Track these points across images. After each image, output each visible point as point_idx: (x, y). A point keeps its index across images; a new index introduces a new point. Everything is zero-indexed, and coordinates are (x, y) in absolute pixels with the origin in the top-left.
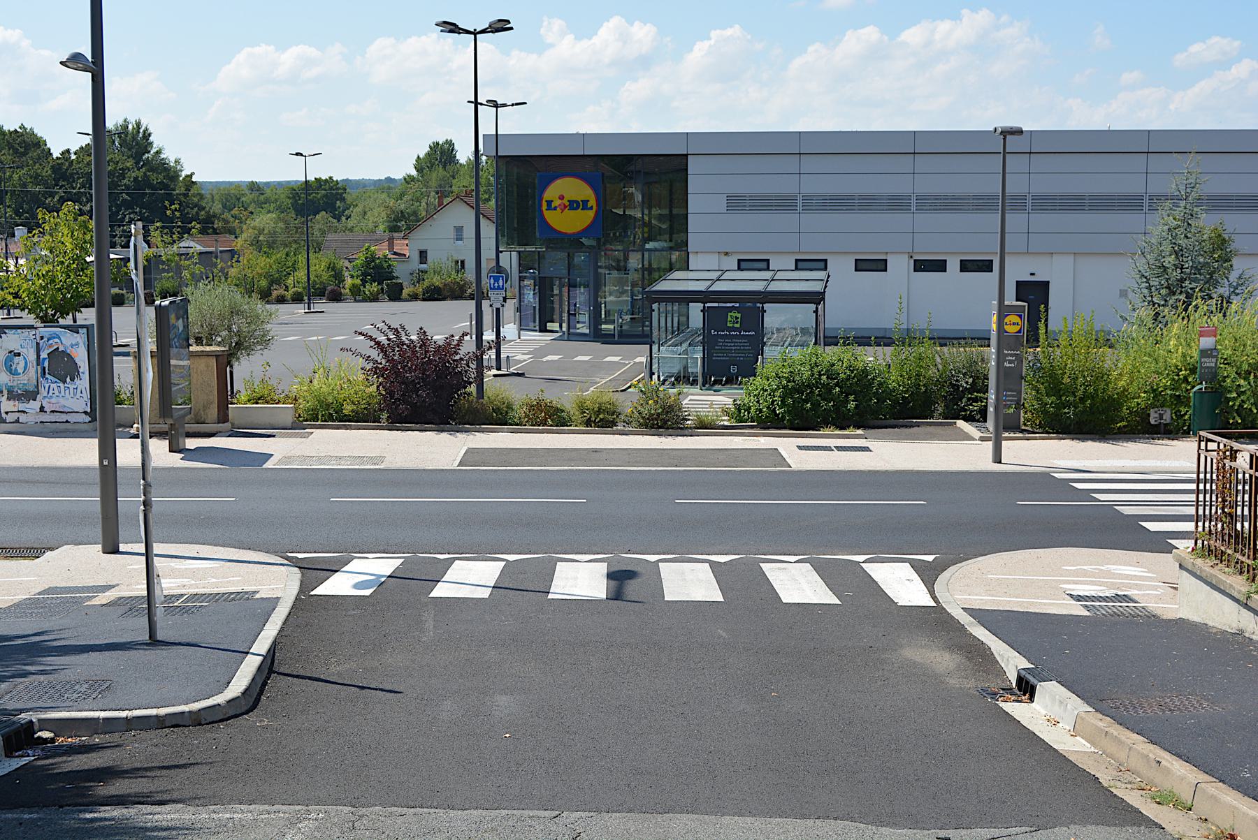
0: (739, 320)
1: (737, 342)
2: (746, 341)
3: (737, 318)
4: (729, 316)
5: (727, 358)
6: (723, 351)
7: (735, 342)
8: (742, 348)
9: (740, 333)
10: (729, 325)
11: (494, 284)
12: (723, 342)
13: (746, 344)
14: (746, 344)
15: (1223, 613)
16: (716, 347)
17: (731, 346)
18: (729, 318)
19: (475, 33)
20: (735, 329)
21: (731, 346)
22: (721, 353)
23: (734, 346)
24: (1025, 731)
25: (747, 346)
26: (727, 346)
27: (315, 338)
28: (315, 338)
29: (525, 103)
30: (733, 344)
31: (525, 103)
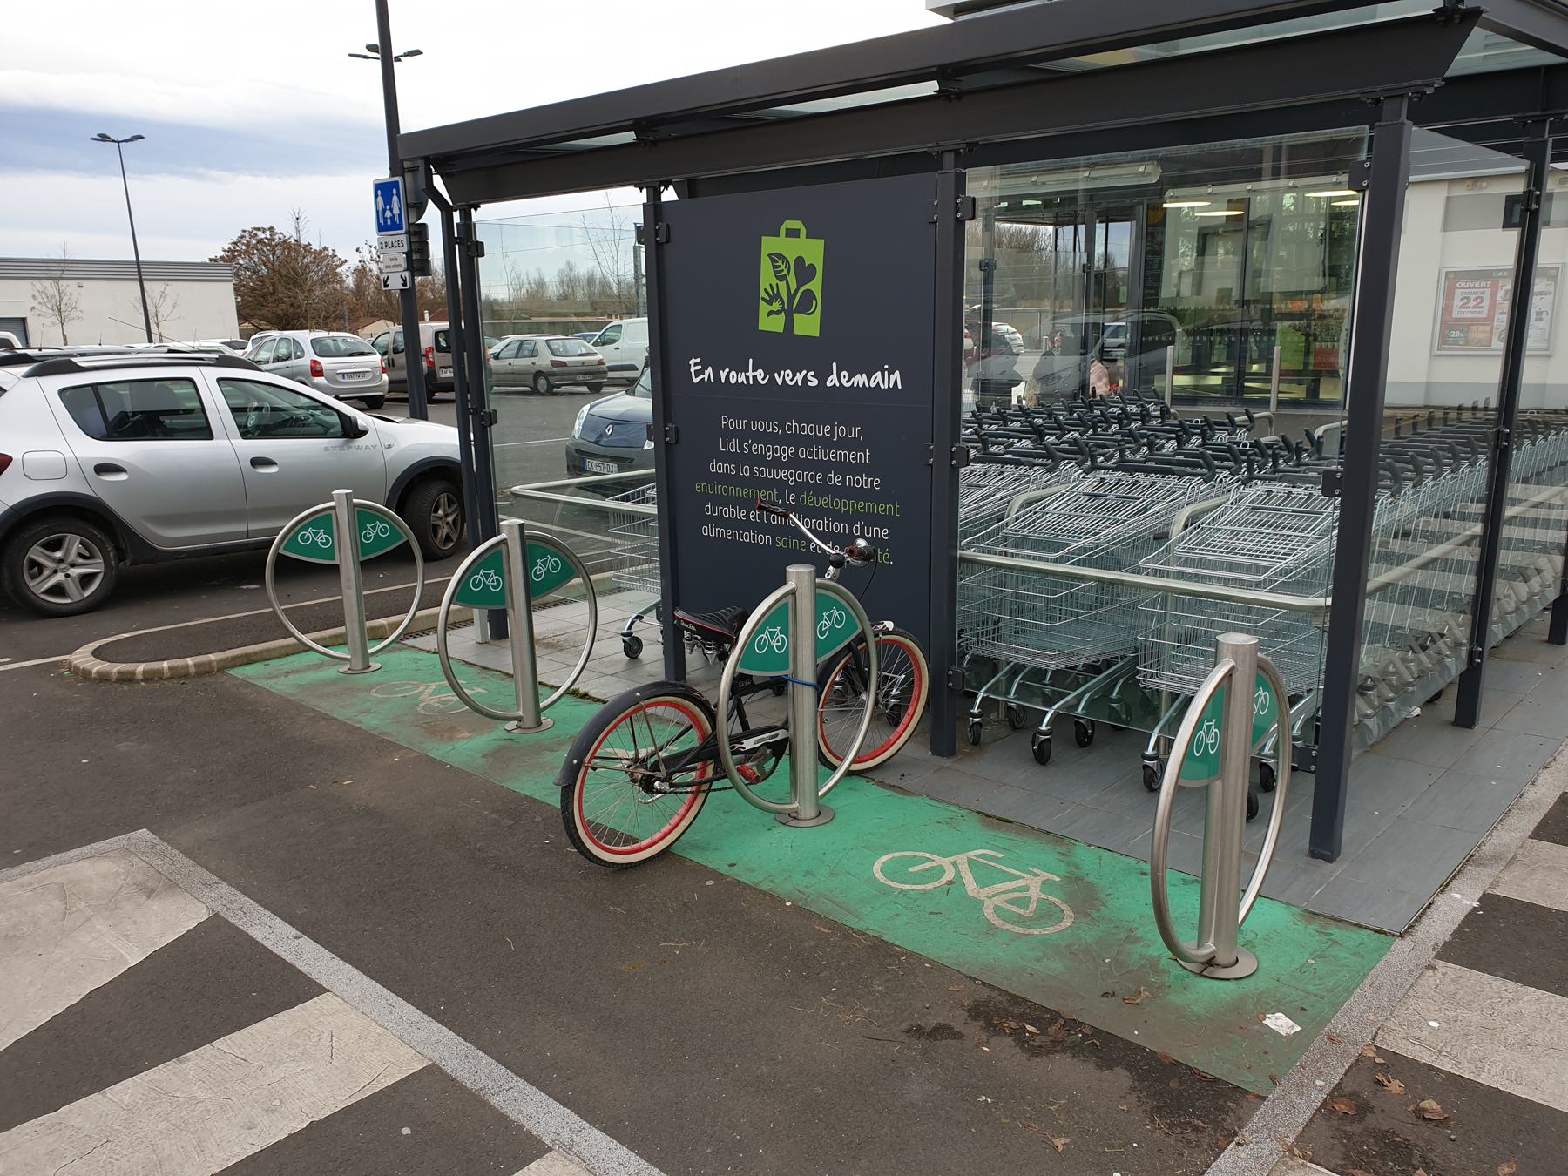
0: (816, 286)
1: (807, 441)
2: (854, 433)
3: (804, 272)
4: (766, 265)
5: (765, 539)
6: (746, 493)
7: (799, 441)
8: (835, 479)
9: (823, 375)
10: (771, 323)
11: (384, 211)
12: (743, 436)
13: (852, 456)
14: (852, 456)
15: (903, 825)
16: (716, 467)
17: (777, 463)
18: (767, 278)
19: (119, 142)
20: (786, 350)
21: (777, 463)
22: (748, 505)
23: (794, 463)
24: (384, 984)
25: (857, 469)
26: (760, 460)
27: (472, 438)
28: (472, 438)
29: (350, 55)
30: (787, 453)
31: (350, 55)
